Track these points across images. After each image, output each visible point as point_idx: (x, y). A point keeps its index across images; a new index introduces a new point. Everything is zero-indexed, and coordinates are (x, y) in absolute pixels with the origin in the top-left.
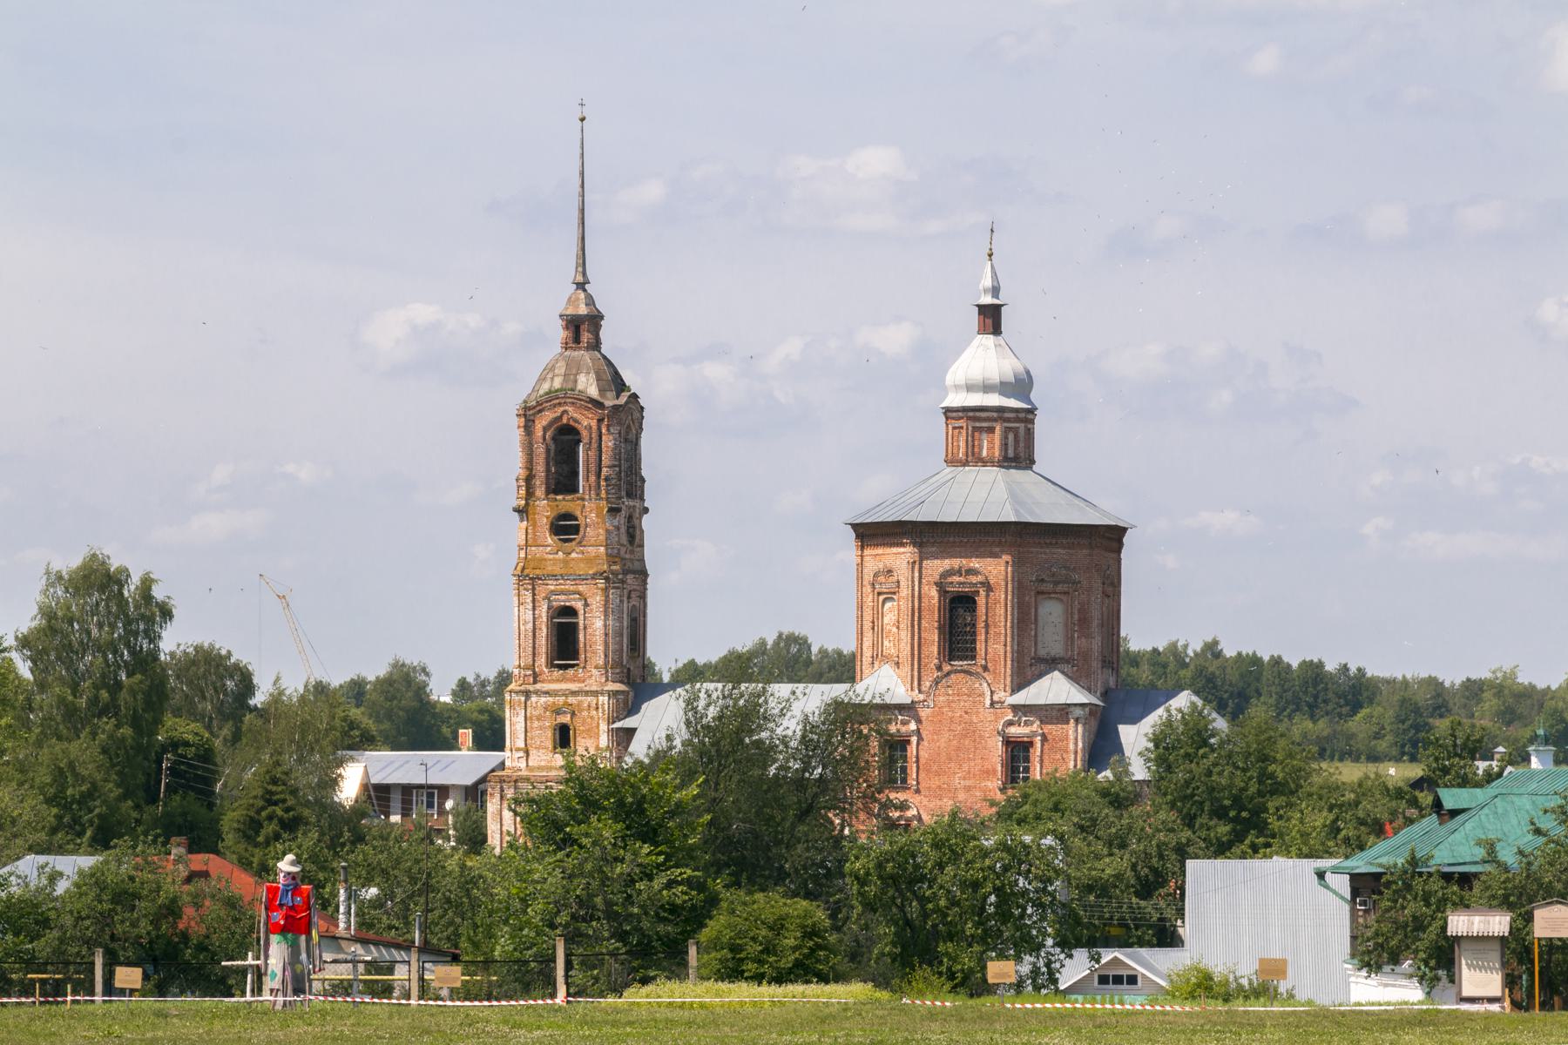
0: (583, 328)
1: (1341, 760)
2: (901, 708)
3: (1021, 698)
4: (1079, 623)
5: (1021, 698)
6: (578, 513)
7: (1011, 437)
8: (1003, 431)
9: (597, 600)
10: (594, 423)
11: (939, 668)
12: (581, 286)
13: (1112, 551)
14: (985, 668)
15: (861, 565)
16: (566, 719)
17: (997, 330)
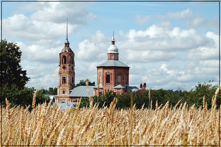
0: (67, 44)
1: (139, 107)
2: (101, 88)
3: (115, 87)
4: (123, 78)
5: (115, 87)
6: (66, 66)
7: (115, 57)
8: (115, 56)
9: (68, 76)
10: (68, 56)
11: (106, 84)
12: (67, 40)
13: (127, 70)
14: (111, 84)
15: (66, 97)
16: (64, 90)
17: (114, 44)
